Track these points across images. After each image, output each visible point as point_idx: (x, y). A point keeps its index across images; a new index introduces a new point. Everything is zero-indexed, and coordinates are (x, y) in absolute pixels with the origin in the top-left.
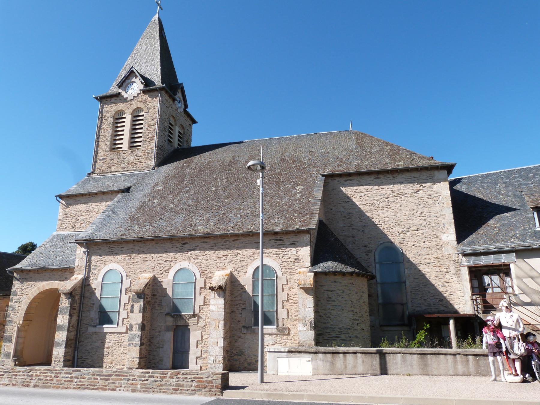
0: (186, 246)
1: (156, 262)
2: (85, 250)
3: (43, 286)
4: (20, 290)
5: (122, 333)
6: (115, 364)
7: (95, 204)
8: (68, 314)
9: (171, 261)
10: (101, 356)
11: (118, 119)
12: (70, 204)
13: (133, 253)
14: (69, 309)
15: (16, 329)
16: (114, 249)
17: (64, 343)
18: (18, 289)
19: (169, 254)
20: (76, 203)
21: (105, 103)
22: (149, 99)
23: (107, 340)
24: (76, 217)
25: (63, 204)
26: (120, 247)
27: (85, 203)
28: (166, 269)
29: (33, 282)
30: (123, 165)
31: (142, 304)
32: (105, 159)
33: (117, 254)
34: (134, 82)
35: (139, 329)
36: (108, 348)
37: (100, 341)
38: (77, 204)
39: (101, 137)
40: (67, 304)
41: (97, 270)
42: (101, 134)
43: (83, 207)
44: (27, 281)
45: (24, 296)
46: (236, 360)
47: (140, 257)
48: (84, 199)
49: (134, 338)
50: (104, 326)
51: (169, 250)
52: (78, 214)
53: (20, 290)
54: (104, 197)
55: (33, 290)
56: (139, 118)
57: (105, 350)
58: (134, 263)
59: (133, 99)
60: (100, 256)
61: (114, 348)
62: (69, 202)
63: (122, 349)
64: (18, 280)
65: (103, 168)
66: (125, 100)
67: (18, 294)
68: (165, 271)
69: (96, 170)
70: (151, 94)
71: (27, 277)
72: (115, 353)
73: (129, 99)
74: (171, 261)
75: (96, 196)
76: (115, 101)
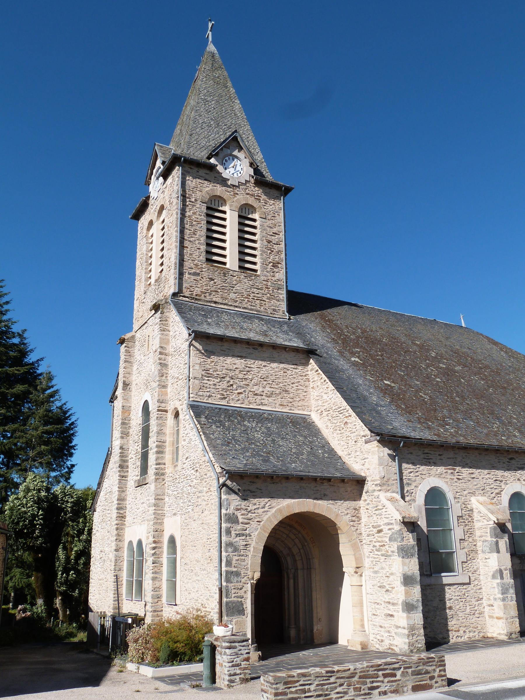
0: (513, 462)
1: (485, 481)
2: (390, 452)
3: (288, 506)
4: (243, 512)
5: (464, 584)
6: (464, 632)
7: (260, 362)
8: (417, 556)
9: (501, 481)
10: (426, 625)
11: (213, 208)
12: (213, 353)
13: (455, 464)
14: (416, 548)
15: (248, 587)
16: (431, 457)
17: (420, 604)
18: (238, 510)
19: (497, 471)
20: (226, 354)
21: (189, 173)
22: (263, 197)
23: (447, 596)
24: (228, 379)
25: (198, 350)
26: (438, 453)
27: (241, 357)
28: (497, 491)
29: (267, 500)
30: (233, 296)
31: (508, 540)
32: (198, 274)
33: (435, 464)
34: (237, 157)
35: (511, 577)
36: (450, 608)
37: (438, 599)
38: (227, 355)
39: (187, 232)
40: (411, 540)
41: (413, 487)
42: (187, 226)
43: (240, 363)
44: (255, 497)
45: (254, 524)
46: (176, 648)
47: (466, 472)
48: (238, 349)
49: (507, 589)
50: (443, 574)
51: (495, 465)
52: (231, 374)
53: (243, 512)
54: (275, 353)
55: (269, 514)
56: (217, 214)
57: (448, 611)
58: (459, 479)
59: (238, 187)
60: (414, 464)
61: (458, 607)
62: (210, 348)
63: (468, 608)
64: (236, 493)
65: (197, 291)
66: (224, 182)
67: (241, 520)
68: (498, 494)
69: (184, 290)
70: (268, 190)
71: (252, 487)
72: (461, 614)
73: (229, 183)
74: (501, 481)
75: (260, 349)
76: (207, 177)
